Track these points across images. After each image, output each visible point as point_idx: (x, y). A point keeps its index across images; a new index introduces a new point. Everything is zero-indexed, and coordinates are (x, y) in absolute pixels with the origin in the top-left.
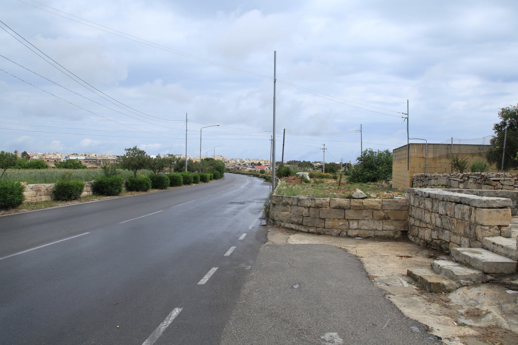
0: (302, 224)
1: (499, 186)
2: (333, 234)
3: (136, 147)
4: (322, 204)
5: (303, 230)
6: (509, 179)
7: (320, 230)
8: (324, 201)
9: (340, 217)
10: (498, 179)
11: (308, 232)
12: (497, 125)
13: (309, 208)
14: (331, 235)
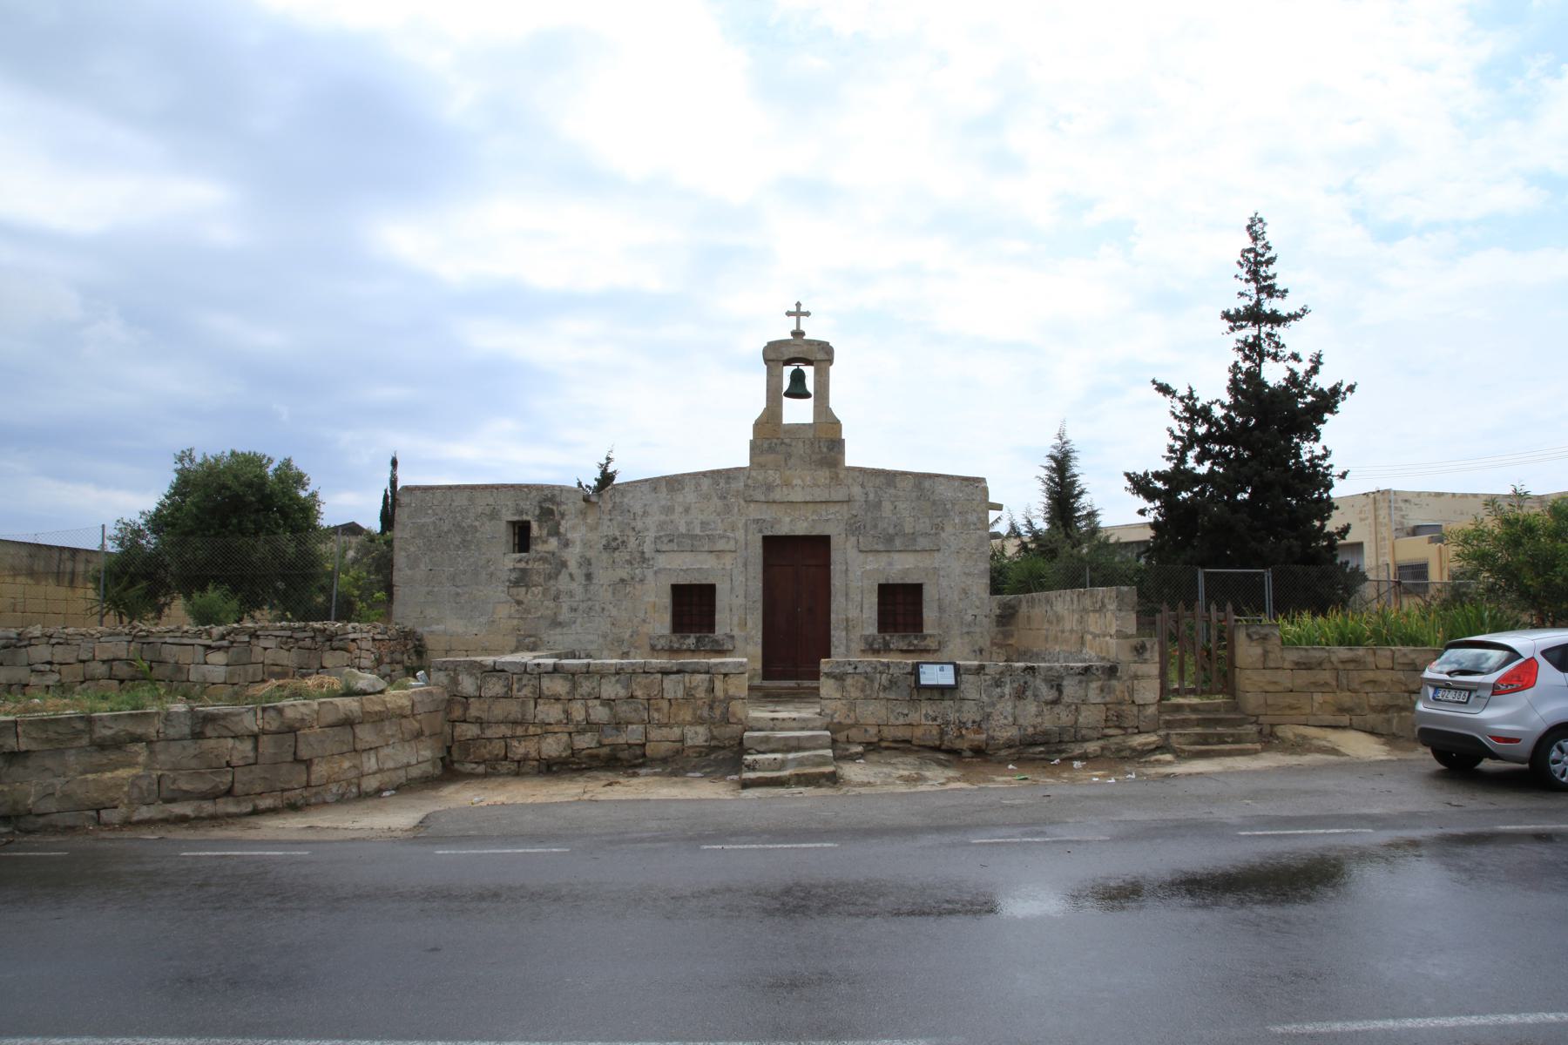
0: (229, 792)
2: (329, 798)
4: (303, 720)
5: (232, 809)
7: (293, 795)
8: (304, 710)
9: (345, 748)
11: (256, 812)
13: (255, 737)
14: (325, 803)
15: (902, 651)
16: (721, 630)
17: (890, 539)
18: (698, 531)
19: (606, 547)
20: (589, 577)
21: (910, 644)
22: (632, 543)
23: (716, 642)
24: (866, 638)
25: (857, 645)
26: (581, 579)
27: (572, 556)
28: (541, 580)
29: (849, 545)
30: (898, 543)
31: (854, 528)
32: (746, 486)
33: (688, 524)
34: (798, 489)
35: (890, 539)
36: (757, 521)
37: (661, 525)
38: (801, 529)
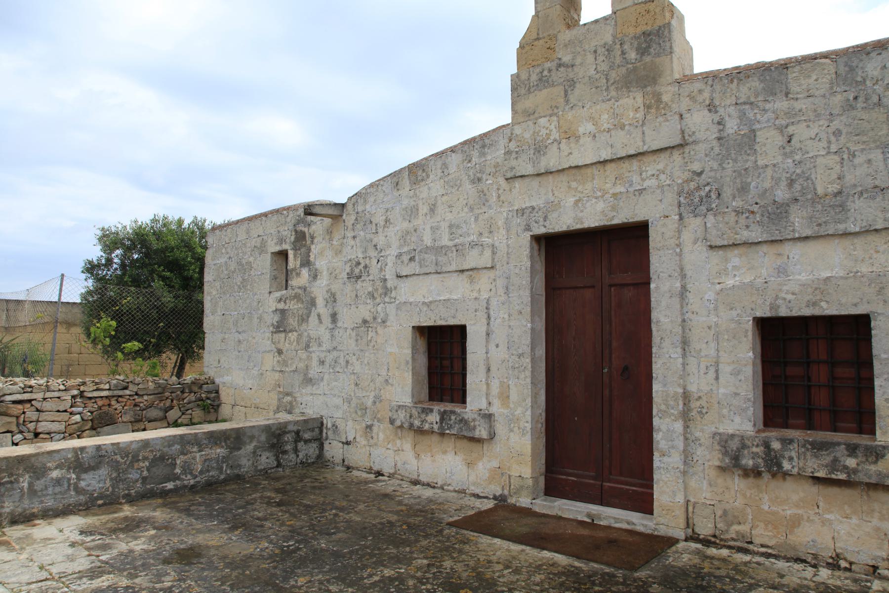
1: (31, 414)
3: (722, 469)
6: (56, 394)
10: (26, 396)
12: (90, 262)
15: (817, 480)
16: (475, 401)
17: (778, 213)
18: (445, 241)
19: (350, 276)
20: (334, 317)
21: (834, 465)
22: (374, 268)
23: (463, 421)
24: (723, 441)
25: (708, 457)
26: (327, 320)
27: (319, 290)
28: (295, 324)
29: (687, 236)
30: (799, 221)
31: (697, 200)
32: (508, 153)
33: (434, 229)
34: (586, 140)
35: (778, 213)
36: (521, 212)
37: (404, 236)
38: (593, 216)
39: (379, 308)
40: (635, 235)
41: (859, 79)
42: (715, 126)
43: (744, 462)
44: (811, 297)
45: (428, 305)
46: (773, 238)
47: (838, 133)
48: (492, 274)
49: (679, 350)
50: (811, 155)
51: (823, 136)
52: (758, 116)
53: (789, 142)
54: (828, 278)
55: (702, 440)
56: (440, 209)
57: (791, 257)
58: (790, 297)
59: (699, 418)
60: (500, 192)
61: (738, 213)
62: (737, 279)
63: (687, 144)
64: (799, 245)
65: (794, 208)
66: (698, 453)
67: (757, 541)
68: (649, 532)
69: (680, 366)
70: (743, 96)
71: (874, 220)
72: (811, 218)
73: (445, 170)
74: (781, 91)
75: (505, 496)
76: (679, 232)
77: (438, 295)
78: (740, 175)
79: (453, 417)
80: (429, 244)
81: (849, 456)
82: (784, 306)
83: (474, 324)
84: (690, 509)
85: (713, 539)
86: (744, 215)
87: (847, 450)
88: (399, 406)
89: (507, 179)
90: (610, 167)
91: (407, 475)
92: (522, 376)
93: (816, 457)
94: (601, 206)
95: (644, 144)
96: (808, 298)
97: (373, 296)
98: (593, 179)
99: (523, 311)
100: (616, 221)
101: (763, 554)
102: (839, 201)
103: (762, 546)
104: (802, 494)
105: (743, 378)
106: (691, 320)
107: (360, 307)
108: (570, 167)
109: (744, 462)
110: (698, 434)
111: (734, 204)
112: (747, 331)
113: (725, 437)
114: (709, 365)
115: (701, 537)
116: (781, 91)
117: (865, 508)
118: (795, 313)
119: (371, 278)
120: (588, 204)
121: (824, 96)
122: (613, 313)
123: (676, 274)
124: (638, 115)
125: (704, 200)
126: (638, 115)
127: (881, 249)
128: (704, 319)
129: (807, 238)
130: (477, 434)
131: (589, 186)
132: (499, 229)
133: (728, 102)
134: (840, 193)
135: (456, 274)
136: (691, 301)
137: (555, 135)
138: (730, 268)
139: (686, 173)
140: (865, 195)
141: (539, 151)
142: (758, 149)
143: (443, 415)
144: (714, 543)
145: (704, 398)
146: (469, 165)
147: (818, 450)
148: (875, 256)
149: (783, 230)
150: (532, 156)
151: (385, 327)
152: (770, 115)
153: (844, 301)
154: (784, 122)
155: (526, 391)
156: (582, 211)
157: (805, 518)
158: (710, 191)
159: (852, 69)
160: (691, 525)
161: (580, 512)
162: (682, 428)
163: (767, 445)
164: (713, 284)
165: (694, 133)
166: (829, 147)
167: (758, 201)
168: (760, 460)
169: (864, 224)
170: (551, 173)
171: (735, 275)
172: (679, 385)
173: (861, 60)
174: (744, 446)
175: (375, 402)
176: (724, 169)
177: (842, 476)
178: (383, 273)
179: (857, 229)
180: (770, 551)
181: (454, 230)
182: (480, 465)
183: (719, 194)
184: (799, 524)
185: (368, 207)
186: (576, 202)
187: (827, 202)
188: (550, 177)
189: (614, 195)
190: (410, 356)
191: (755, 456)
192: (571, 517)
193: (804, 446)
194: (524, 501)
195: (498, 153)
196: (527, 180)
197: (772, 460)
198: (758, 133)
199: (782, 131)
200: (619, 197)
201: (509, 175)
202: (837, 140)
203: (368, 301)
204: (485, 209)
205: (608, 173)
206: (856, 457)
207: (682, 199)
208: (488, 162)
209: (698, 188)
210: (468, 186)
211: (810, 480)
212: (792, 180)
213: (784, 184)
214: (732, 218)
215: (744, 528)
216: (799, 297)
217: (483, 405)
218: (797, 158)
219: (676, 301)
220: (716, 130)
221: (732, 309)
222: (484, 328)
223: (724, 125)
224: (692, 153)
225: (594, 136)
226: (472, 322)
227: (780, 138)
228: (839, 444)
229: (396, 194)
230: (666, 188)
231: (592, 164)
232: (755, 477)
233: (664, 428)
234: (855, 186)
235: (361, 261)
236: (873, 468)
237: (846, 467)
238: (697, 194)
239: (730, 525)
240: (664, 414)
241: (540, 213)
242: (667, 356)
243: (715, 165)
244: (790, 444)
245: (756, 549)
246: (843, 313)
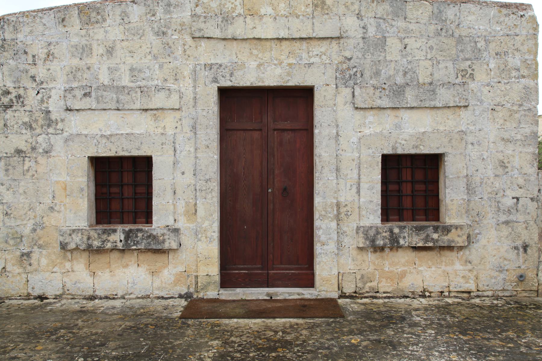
17: (398, 91)
18: (126, 81)
21: (427, 238)
22: (32, 99)
24: (366, 231)
25: (353, 241)
29: (340, 100)
30: (410, 97)
31: (348, 76)
32: (194, 16)
35: (398, 91)
38: (272, 77)
39: (40, 139)
40: (305, 94)
41: (444, 19)
42: (361, 29)
43: (378, 243)
44: (415, 143)
45: (108, 138)
46: (396, 106)
47: (431, 48)
48: (177, 114)
49: (334, 175)
50: (417, 58)
51: (424, 48)
52: (388, 29)
53: (405, 48)
54: (424, 132)
55: (348, 232)
56: (119, 52)
57: (403, 118)
58: (403, 142)
59: (346, 219)
60: (186, 47)
61: (375, 88)
62: (371, 129)
63: (342, 38)
64: (409, 111)
65: (408, 89)
66: (345, 241)
67: (381, 290)
68: (314, 297)
69: (334, 185)
70: (379, 13)
71: (449, 101)
72: (417, 96)
73: (126, 18)
74: (402, 16)
75: (191, 293)
76: (336, 96)
77: (118, 129)
78: (375, 64)
79: (140, 235)
80: (106, 83)
81: (434, 232)
82: (400, 148)
83: (161, 155)
84: (340, 278)
85: (354, 295)
86: (379, 90)
87: (434, 229)
88: (74, 231)
89: (193, 38)
90: (284, 43)
91: (79, 293)
92: (210, 196)
93: (418, 235)
94: (278, 71)
95: (314, 32)
96: (414, 143)
97: (31, 127)
98: (272, 50)
99: (210, 146)
100: (290, 84)
101: (385, 298)
102: (431, 87)
103: (384, 293)
104: (407, 258)
105: (375, 192)
106: (341, 155)
107: (10, 136)
108: (254, 38)
109: (378, 243)
110: (345, 229)
111: (371, 82)
112: (378, 162)
113: (366, 229)
114: (352, 184)
115: (347, 294)
116: (402, 16)
117: (438, 261)
118: (406, 152)
119: (28, 108)
120: (269, 68)
121: (425, 24)
122: (275, 149)
123: (333, 124)
124: (308, 10)
125: (353, 77)
126: (308, 10)
127: (450, 118)
128: (350, 154)
129: (413, 108)
130: (166, 246)
131: (267, 55)
132: (184, 78)
133: (370, 15)
134: (431, 84)
135: (139, 112)
136: (342, 143)
137: (239, 10)
138: (367, 123)
139: (341, 57)
140: (445, 87)
141: (227, 21)
142: (387, 49)
143: (128, 235)
144: (356, 297)
145: (349, 205)
146: (153, 18)
147: (419, 231)
148: (447, 121)
149: (401, 102)
150: (219, 23)
151: (50, 157)
152: (395, 29)
153: (432, 145)
154: (403, 36)
155: (213, 208)
156: (263, 73)
157: (408, 271)
158: (356, 72)
159: (440, 12)
160: (341, 289)
161: (261, 294)
162: (336, 226)
163: (391, 231)
164: (356, 132)
165: (347, 31)
166: (426, 56)
167: (386, 82)
168: (387, 241)
169: (444, 103)
170: (236, 39)
171: (370, 127)
172: (334, 198)
173: (445, 8)
174: (378, 233)
175: (34, 230)
176: (365, 58)
177: (431, 244)
178: (45, 105)
179: (441, 106)
180: (388, 295)
181: (136, 73)
182: (166, 272)
183: (362, 75)
184: (405, 275)
185: (21, 37)
186: (259, 65)
187: (426, 88)
188: (235, 43)
189: (290, 65)
190: (86, 184)
191: (385, 237)
192: (254, 298)
193: (411, 229)
194: (212, 293)
195: (183, 14)
196: (212, 41)
197: (394, 240)
198: (387, 39)
199: (401, 41)
200: (293, 66)
201: (197, 35)
202: (431, 52)
203: (24, 131)
204: (169, 59)
205: (283, 47)
206: (438, 233)
207: (337, 74)
208: (174, 20)
209: (348, 69)
210: (151, 37)
211: (411, 249)
212: (406, 72)
213: (401, 73)
214: (371, 91)
215: (373, 284)
216: (409, 142)
217: (170, 222)
218: (409, 59)
219: (333, 141)
220: (361, 32)
221: (369, 148)
222: (172, 159)
223: (367, 30)
224: (345, 44)
225: (275, 18)
226: (159, 154)
227: (400, 45)
228: (429, 226)
229: (61, 29)
230: (328, 65)
231: (271, 39)
232: (380, 251)
233: (324, 226)
234: (439, 80)
235: (11, 90)
236: (446, 238)
237: (433, 239)
238: (348, 73)
239: (365, 284)
240: (323, 217)
241: (227, 70)
242: (326, 178)
243: (360, 56)
244: (404, 229)
245: (380, 295)
246: (431, 153)
